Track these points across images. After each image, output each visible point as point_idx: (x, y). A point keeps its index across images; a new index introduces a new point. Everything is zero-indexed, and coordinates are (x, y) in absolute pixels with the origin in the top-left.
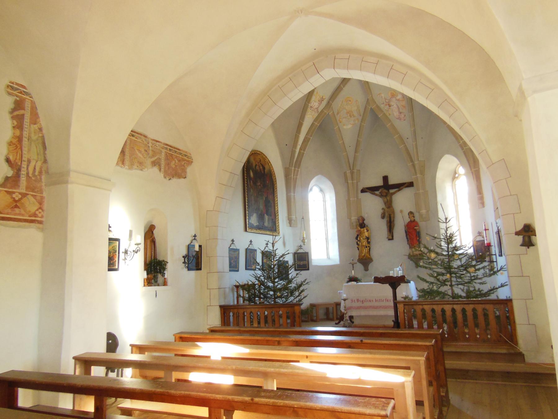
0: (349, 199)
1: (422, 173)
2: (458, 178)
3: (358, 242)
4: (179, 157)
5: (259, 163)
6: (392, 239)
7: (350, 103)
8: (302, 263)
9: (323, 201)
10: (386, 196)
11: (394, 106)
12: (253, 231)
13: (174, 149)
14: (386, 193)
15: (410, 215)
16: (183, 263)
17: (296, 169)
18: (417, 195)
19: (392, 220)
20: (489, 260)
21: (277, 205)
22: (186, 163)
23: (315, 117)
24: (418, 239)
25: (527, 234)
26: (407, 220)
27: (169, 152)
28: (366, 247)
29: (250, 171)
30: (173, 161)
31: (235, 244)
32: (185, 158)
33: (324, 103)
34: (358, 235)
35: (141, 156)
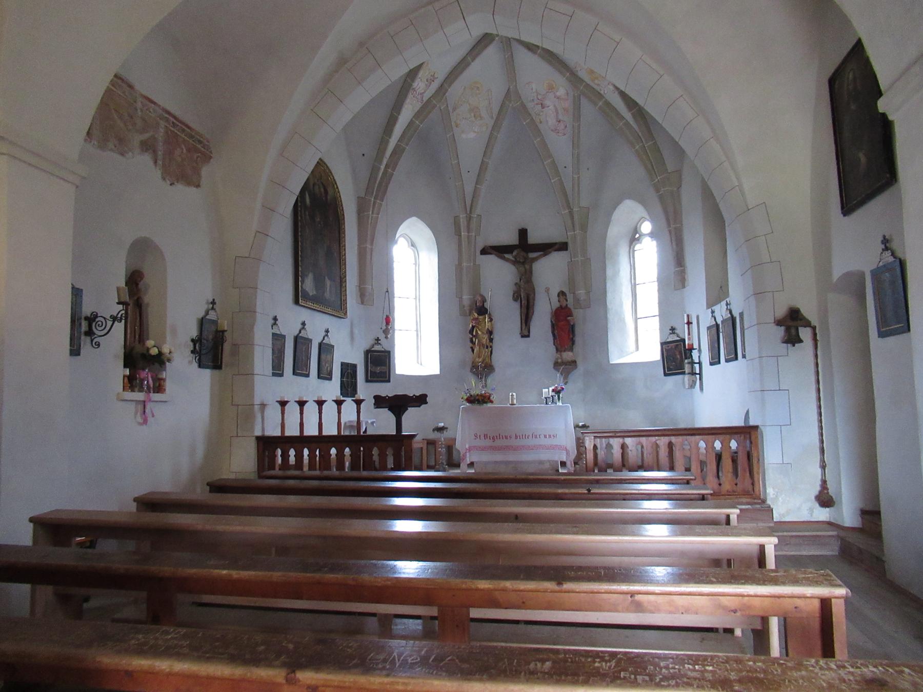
1: (584, 228)
2: (639, 240)
4: (189, 141)
6: (528, 336)
8: (378, 369)
9: (415, 264)
10: (523, 263)
16: (192, 352)
17: (378, 201)
18: (571, 265)
19: (531, 304)
23: (416, 110)
24: (571, 336)
26: (556, 304)
27: (172, 129)
30: (178, 149)
31: (279, 325)
32: (199, 146)
33: (435, 85)
34: (473, 327)
35: (122, 125)
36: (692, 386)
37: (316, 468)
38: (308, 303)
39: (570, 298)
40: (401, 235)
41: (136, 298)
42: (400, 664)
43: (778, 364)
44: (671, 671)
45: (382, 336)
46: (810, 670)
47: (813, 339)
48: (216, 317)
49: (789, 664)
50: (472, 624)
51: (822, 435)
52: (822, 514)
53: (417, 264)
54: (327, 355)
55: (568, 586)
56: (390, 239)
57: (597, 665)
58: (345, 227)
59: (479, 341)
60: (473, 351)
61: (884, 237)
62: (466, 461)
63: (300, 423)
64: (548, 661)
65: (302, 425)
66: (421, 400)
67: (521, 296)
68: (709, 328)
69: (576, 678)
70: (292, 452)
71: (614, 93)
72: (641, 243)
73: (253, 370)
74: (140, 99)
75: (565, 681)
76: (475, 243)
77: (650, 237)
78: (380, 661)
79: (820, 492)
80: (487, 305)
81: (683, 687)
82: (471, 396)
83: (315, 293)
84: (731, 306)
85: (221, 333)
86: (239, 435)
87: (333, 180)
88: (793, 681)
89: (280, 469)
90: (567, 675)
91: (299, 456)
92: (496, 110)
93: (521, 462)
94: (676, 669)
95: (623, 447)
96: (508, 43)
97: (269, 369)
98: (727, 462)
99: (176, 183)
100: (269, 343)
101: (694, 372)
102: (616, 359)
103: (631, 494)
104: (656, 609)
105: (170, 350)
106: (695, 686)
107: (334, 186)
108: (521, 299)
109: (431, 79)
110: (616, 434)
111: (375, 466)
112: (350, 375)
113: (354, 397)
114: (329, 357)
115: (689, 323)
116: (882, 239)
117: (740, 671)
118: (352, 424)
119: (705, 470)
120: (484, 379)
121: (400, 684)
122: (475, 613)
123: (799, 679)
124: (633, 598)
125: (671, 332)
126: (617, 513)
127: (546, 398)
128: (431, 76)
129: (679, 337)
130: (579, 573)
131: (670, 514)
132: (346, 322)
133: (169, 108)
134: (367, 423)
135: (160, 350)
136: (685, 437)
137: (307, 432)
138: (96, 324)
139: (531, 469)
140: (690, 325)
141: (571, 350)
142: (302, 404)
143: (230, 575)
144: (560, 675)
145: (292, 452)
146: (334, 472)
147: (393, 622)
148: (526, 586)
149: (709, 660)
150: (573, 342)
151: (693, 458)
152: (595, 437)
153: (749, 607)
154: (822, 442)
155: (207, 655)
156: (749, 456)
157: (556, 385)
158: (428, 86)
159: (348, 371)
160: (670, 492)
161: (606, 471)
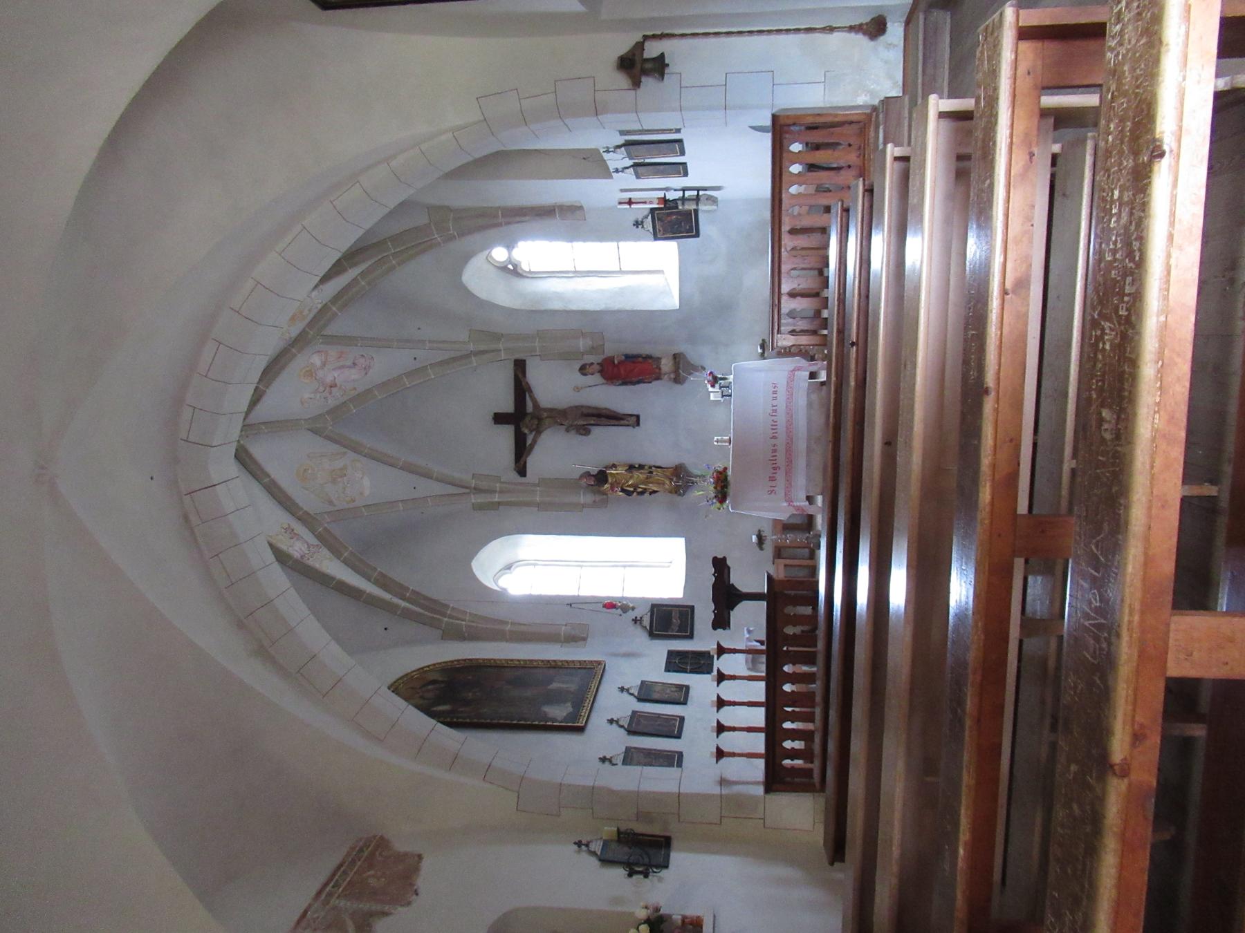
0: (538, 505)
1: (497, 337)
2: (516, 265)
3: (640, 490)
4: (360, 866)
6: (638, 417)
8: (676, 621)
9: (535, 565)
11: (336, 375)
12: (585, 713)
14: (532, 419)
16: (646, 876)
17: (449, 612)
19: (595, 412)
20: (695, 202)
24: (640, 359)
25: (638, 66)
26: (597, 378)
28: (651, 472)
29: (434, 711)
30: (369, 882)
31: (611, 755)
33: (299, 528)
34: (623, 490)
36: (713, 200)
37: (811, 712)
38: (583, 714)
40: (496, 584)
42: (1101, 617)
43: (711, 86)
44: (1119, 245)
45: (631, 615)
46: (1122, 59)
47: (661, 39)
48: (599, 842)
49: (1113, 87)
50: (1034, 512)
51: (788, 31)
52: (895, 31)
53: (534, 563)
54: (655, 691)
55: (990, 380)
56: (498, 598)
57: (1108, 347)
58: (481, 659)
59: (642, 483)
60: (655, 492)
62: (805, 506)
63: (748, 731)
64: (1101, 413)
65: (750, 730)
66: (720, 565)
67: (584, 425)
68: (638, 177)
69: (1127, 376)
70: (788, 744)
71: (322, 290)
72: (520, 262)
73: (673, 794)
75: (1130, 392)
76: (509, 483)
77: (512, 250)
78: (1097, 646)
79: (865, 33)
80: (594, 471)
81: (1143, 230)
82: (716, 497)
84: (610, 146)
85: (622, 836)
86: (763, 817)
87: (418, 672)
88: (1139, 82)
89: (812, 762)
90: (1121, 390)
91: (794, 735)
92: (334, 448)
93: (809, 430)
94: (1116, 240)
95: (792, 295)
96: (247, 428)
97: (673, 772)
98: (821, 157)
99: (415, 887)
100: (635, 770)
101: (695, 197)
102: (672, 301)
103: (859, 288)
104: (1027, 261)
105: (643, 908)
106: (1143, 215)
107: (426, 671)
108: (586, 425)
109: (290, 533)
110: (775, 304)
111: (809, 632)
112: (682, 661)
113: (713, 656)
114: (658, 688)
115: (630, 202)
117: (1121, 153)
118: (750, 661)
119: (827, 186)
120: (694, 479)
121: (1131, 619)
122: (1022, 508)
123: (1135, 74)
124: (1010, 292)
125: (640, 227)
126: (886, 306)
127: (723, 396)
128: (286, 532)
129: (648, 215)
130: (972, 364)
131: (890, 236)
132: (611, 664)
133: (314, 893)
134: (749, 640)
135: (642, 921)
136: (783, 212)
137: (761, 723)
139: (819, 419)
140: (633, 200)
141: (659, 359)
142: (721, 728)
143: (966, 843)
144: (1121, 398)
145: (788, 744)
146: (816, 687)
147: (1031, 615)
148: (989, 438)
149: (1105, 194)
150: (649, 357)
151: (813, 202)
152: (779, 332)
153: (1027, 135)
154: (797, 30)
155: (1086, 886)
156: (812, 128)
157: (706, 382)
159: (677, 662)
160: (859, 235)
161: (827, 319)
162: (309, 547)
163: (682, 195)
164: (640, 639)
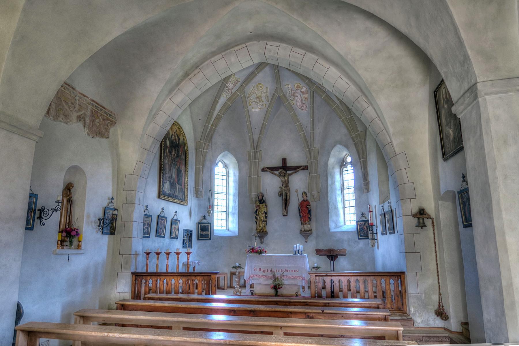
2: (345, 166)
3: (257, 217)
4: (104, 115)
5: (175, 133)
6: (287, 215)
7: (261, 89)
10: (284, 176)
13: (99, 107)
15: (304, 195)
17: (207, 143)
19: (288, 198)
21: (188, 176)
22: (110, 123)
23: (228, 97)
24: (309, 216)
26: (301, 199)
27: (95, 109)
28: (264, 221)
33: (238, 85)
34: (257, 210)
35: (67, 108)
36: (373, 246)
39: (309, 195)
41: (68, 197)
45: (207, 215)
56: (214, 164)
60: (256, 223)
61: (463, 174)
74: (78, 95)
83: (170, 192)
101: (374, 238)
114: (177, 227)
116: (462, 175)
127: (298, 250)
128: (236, 80)
138: (44, 213)
150: (310, 219)
158: (234, 86)
162: (231, 89)
163: (374, 232)
164: (196, 218)
